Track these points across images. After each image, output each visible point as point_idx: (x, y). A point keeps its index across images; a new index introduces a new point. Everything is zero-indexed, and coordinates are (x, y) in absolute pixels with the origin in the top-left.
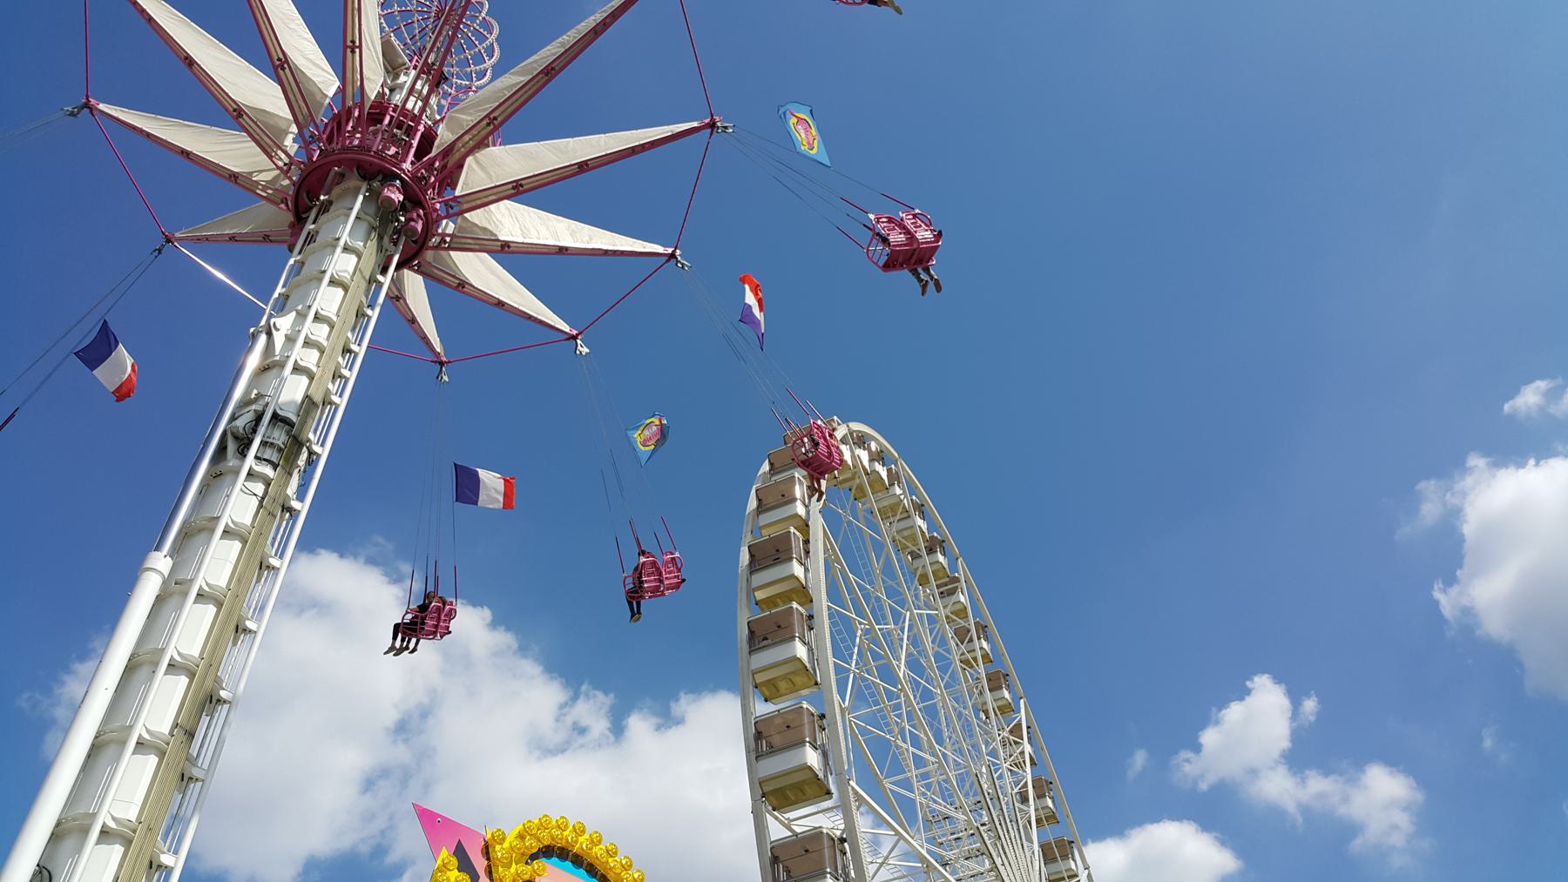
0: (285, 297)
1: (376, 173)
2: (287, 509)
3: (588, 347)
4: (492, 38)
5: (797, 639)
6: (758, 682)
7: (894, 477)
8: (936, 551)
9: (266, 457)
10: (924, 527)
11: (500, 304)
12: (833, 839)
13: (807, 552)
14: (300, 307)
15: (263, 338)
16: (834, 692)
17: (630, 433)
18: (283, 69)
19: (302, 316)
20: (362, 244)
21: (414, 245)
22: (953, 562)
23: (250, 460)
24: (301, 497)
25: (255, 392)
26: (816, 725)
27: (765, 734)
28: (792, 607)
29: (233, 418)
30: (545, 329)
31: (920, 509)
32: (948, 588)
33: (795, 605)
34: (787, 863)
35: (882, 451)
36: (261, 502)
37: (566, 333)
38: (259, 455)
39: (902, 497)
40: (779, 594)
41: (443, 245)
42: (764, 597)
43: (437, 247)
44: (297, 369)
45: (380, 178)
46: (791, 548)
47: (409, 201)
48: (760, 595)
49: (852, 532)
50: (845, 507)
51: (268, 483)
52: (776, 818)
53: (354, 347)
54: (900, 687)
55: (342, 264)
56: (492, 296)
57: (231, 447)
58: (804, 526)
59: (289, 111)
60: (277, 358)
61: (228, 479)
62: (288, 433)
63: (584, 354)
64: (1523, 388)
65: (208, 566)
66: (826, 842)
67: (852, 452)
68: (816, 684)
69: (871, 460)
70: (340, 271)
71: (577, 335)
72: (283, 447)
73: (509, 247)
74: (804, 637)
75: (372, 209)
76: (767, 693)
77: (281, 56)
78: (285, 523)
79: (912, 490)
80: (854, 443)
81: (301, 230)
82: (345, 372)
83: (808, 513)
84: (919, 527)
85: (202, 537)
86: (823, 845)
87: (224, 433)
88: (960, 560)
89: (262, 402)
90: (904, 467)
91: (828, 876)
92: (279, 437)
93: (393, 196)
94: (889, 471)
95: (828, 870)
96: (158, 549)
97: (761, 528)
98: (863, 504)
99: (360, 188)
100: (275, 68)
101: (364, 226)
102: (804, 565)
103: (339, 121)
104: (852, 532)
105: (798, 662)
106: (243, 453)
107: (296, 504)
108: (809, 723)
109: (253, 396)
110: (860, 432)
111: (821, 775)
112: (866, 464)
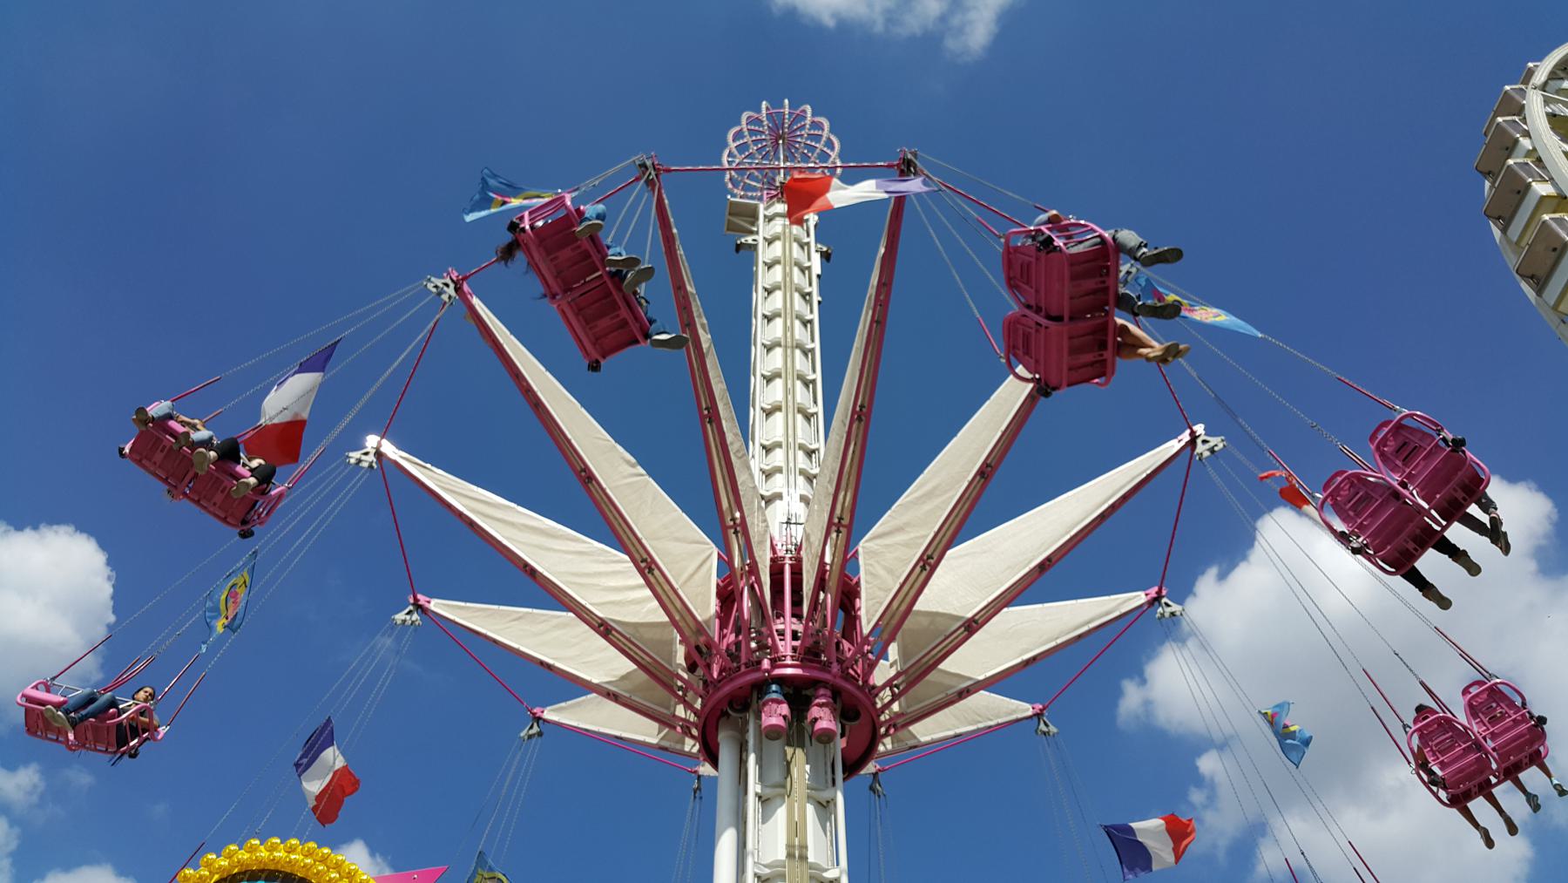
4: (826, 133)
30: (1167, 470)
37: (1182, 448)
56: (1015, 584)
59: (663, 612)
64: (1259, 524)
77: (645, 556)
97: (1518, 243)
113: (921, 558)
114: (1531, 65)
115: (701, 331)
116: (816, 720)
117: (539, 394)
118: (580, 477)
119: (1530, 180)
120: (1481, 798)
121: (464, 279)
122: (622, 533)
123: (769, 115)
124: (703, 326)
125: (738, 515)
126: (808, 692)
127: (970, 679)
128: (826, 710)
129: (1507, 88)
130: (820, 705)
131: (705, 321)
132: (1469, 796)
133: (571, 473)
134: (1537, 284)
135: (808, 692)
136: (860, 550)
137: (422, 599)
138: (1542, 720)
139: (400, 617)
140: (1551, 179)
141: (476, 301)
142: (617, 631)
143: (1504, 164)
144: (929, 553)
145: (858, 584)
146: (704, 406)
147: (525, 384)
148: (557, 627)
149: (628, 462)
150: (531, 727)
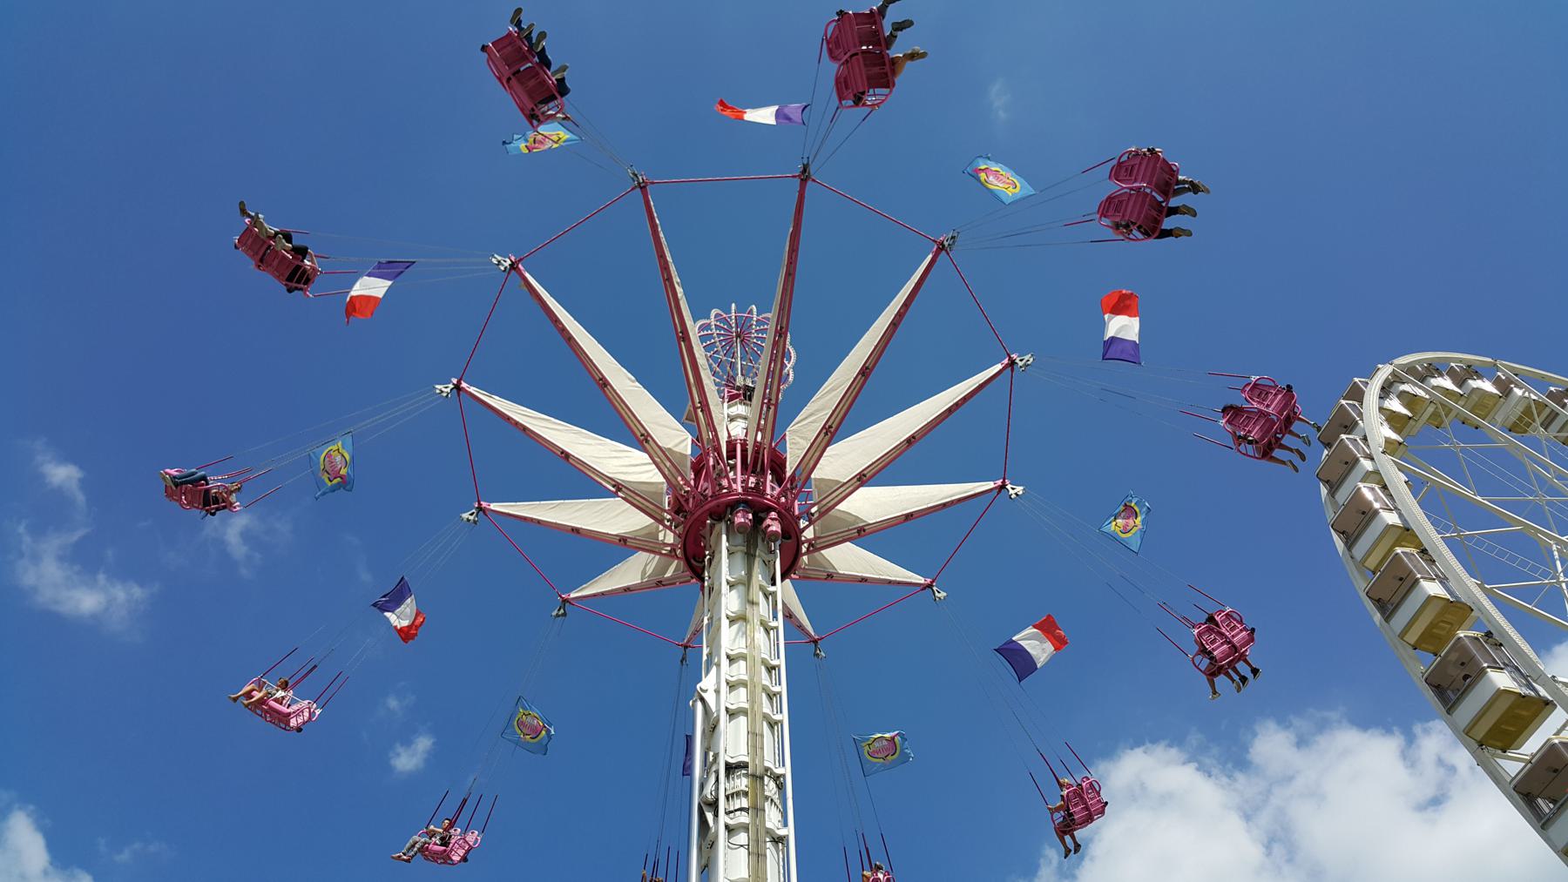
1: (723, 512)
3: (1021, 486)
7: (1505, 388)
9: (737, 807)
15: (699, 705)
17: (1105, 529)
25: (711, 754)
28: (1397, 554)
29: (702, 787)
33: (1461, 634)
35: (1469, 366)
39: (1527, 394)
41: (813, 518)
42: (1379, 615)
44: (732, 714)
45: (729, 511)
46: (1411, 571)
49: (1561, 510)
50: (1534, 491)
57: (709, 816)
59: (646, 517)
62: (747, 775)
63: (1021, 493)
71: (1004, 482)
72: (747, 789)
73: (865, 475)
77: (644, 432)
78: (781, 853)
87: (699, 804)
90: (1505, 368)
92: (742, 783)
100: (641, 442)
105: (1394, 529)
113: (824, 427)
115: (676, 286)
116: (769, 526)
117: (571, 332)
118: (599, 384)
119: (1419, 576)
120: (1242, 662)
121: (521, 260)
124: (678, 283)
126: (762, 515)
127: (865, 521)
128: (777, 522)
129: (1356, 380)
130: (772, 519)
131: (679, 280)
133: (594, 383)
134: (1331, 488)
135: (762, 515)
136: (787, 433)
137: (484, 504)
139: (465, 516)
140: (1396, 508)
141: (528, 275)
142: (625, 487)
144: (829, 423)
145: (786, 458)
146: (679, 330)
147: (561, 326)
148: (600, 444)
149: (629, 379)
150: (559, 610)
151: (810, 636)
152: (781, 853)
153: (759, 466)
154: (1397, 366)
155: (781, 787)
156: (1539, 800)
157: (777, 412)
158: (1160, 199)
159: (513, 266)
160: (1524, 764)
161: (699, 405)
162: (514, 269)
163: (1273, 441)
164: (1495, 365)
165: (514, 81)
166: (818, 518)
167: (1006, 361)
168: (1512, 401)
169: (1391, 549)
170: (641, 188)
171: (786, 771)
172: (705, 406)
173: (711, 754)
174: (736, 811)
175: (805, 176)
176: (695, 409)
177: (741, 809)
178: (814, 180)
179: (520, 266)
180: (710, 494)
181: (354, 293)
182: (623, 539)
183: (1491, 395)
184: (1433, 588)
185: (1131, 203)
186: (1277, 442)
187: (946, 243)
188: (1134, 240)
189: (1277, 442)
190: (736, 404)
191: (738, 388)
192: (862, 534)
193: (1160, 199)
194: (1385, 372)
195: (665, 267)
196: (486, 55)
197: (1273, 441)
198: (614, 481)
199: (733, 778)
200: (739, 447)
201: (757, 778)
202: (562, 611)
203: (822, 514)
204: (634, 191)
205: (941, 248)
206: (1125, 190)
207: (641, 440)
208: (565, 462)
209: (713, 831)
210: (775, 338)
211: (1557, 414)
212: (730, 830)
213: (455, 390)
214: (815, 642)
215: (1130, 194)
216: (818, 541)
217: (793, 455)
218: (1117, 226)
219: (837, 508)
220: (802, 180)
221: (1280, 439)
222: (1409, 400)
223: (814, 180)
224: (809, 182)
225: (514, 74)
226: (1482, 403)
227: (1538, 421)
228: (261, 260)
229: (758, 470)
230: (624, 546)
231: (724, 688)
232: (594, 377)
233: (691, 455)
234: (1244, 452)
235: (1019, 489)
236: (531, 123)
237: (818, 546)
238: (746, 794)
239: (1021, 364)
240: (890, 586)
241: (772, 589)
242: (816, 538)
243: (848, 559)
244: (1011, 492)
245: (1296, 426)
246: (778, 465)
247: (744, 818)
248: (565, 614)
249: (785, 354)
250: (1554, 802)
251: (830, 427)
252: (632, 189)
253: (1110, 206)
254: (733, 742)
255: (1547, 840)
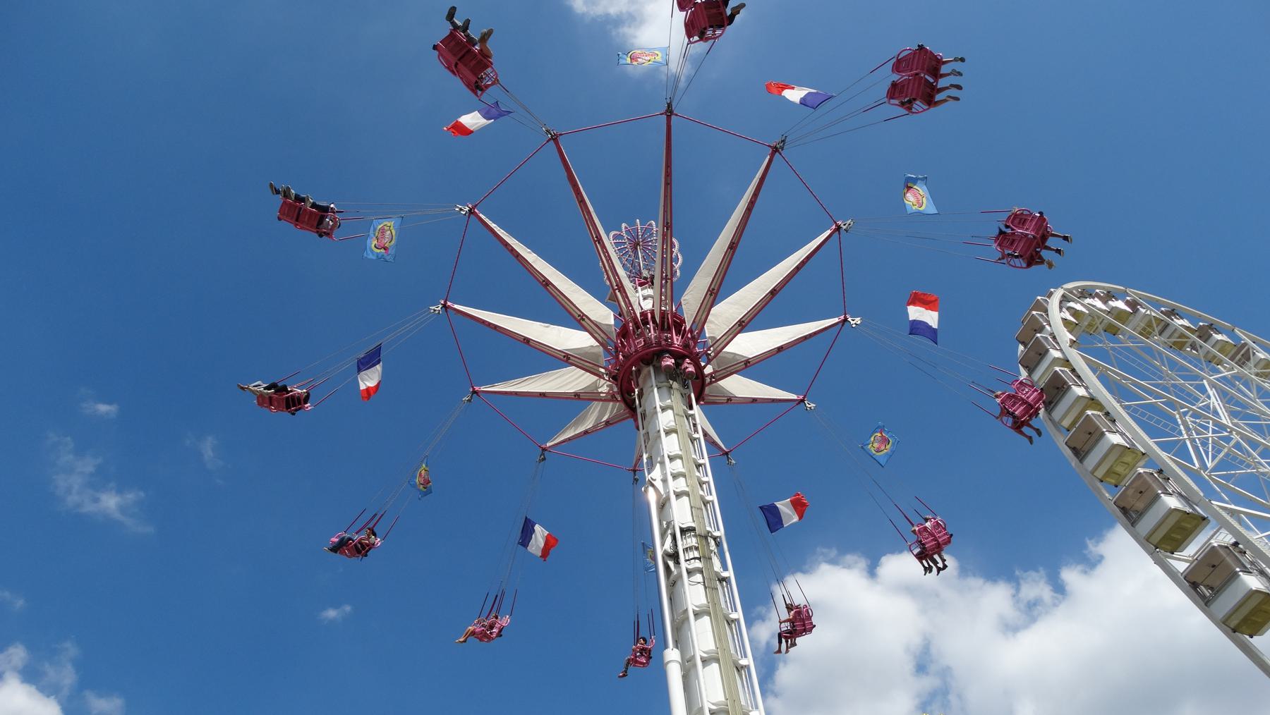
0: (650, 458)
1: (651, 357)
2: (722, 580)
5: (1162, 495)
6: (1099, 477)
7: (1133, 305)
8: (1212, 335)
9: (691, 557)
10: (1185, 323)
11: (780, 349)
12: (1227, 547)
13: (1079, 377)
14: (659, 459)
16: (1147, 440)
18: (584, 320)
19: (662, 463)
20: (670, 401)
21: (697, 381)
22: (1231, 334)
23: (684, 565)
24: (725, 568)
25: (665, 523)
26: (1160, 480)
27: (1128, 507)
28: (1088, 415)
31: (1172, 313)
32: (1242, 355)
34: (1205, 583)
35: (1109, 292)
36: (704, 585)
38: (687, 558)
39: (1148, 312)
40: (1171, 529)
43: (711, 383)
44: (678, 495)
45: (656, 358)
47: (679, 359)
48: (1066, 423)
49: (1121, 354)
51: (700, 571)
52: (1179, 559)
53: (701, 461)
54: (1229, 430)
55: (665, 419)
57: (671, 564)
58: (1066, 362)
60: (664, 496)
61: (679, 583)
62: (695, 536)
63: (859, 322)
65: (698, 640)
66: (1222, 552)
67: (1082, 305)
68: (1144, 454)
69: (1105, 303)
70: (668, 424)
74: (1167, 490)
75: (663, 377)
76: (1113, 481)
77: (579, 313)
78: (726, 589)
79: (1157, 305)
80: (1078, 298)
81: (637, 415)
82: (705, 479)
83: (1063, 353)
84: (1181, 325)
85: (686, 625)
86: (1222, 556)
87: (663, 558)
88: (1236, 331)
89: (671, 527)
90: (1133, 293)
91: (1241, 573)
92: (692, 541)
93: (668, 363)
94: (1127, 303)
95: (1238, 569)
96: (666, 647)
98: (1124, 335)
99: (650, 371)
100: (579, 321)
101: (665, 390)
102: (1083, 386)
103: (624, 333)
104: (1121, 354)
106: (677, 563)
107: (725, 574)
108: (1153, 481)
109: (665, 526)
110: (1078, 287)
111: (1188, 510)
112: (1104, 307)
114: (1052, 290)
121: (476, 206)
122: (568, 307)
123: (628, 232)
124: (575, 431)
125: (663, 290)
129: (1039, 298)
132: (932, 97)
133: (540, 284)
136: (682, 302)
138: (921, 47)
142: (573, 356)
143: (1034, 335)
151: (720, 448)
152: (726, 589)
153: (666, 324)
154: (1066, 290)
155: (718, 544)
156: (1202, 587)
157: (672, 287)
158: (932, 80)
159: (471, 212)
160: (1189, 564)
161: (616, 287)
162: (472, 213)
163: (1034, 253)
164: (1126, 291)
165: (461, 66)
166: (715, 357)
167: (834, 227)
168: (1138, 317)
169: (1082, 412)
170: (554, 139)
171: (720, 533)
172: (621, 287)
173: (665, 523)
174: (691, 559)
175: (669, 112)
176: (614, 290)
177: (695, 558)
178: (676, 115)
179: (476, 210)
180: (634, 350)
181: (379, 367)
182: (577, 395)
183: (1125, 311)
184: (1115, 439)
185: (911, 85)
186: (1037, 254)
187: (778, 146)
188: (916, 113)
189: (1037, 254)
190: (646, 288)
191: (645, 278)
192: (747, 367)
193: (932, 80)
194: (1058, 294)
195: (582, 201)
196: (436, 53)
197: (1034, 253)
198: (564, 353)
199: (685, 538)
200: (649, 315)
201: (705, 537)
202: (542, 457)
203: (717, 354)
204: (550, 142)
205: (775, 150)
206: (905, 78)
207: (578, 321)
208: (526, 346)
209: (675, 573)
210: (663, 230)
211: (1168, 324)
212: (690, 572)
213: (444, 308)
214: (726, 454)
215: (910, 80)
216: (717, 374)
217: (689, 316)
218: (902, 104)
219: (724, 350)
220: (668, 116)
221: (1039, 252)
222: (1075, 313)
223: (676, 115)
224: (673, 117)
225: (459, 60)
226: (1119, 314)
227: (1157, 330)
228: (297, 220)
229: (666, 327)
230: (581, 399)
231: (670, 478)
232: (539, 281)
233: (615, 325)
234: (1014, 265)
235: (858, 320)
236: (476, 94)
237: (718, 378)
238: (697, 548)
239: (844, 227)
240: (773, 404)
241: (691, 412)
242: (715, 372)
243: (738, 386)
244: (852, 322)
245: (1051, 242)
246: (679, 324)
247: (698, 564)
248: (544, 459)
249: (672, 246)
250: (1212, 588)
251: (713, 289)
252: (548, 141)
253: (895, 91)
254: (681, 514)
255: (1211, 616)
